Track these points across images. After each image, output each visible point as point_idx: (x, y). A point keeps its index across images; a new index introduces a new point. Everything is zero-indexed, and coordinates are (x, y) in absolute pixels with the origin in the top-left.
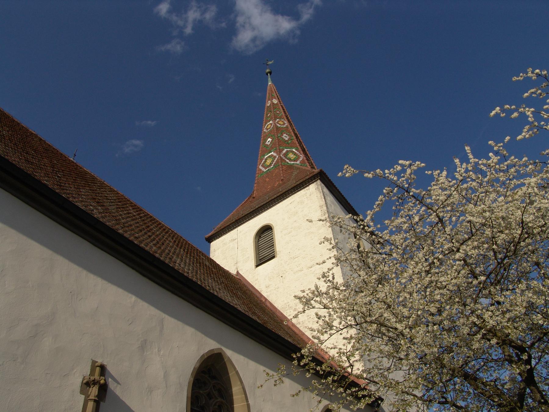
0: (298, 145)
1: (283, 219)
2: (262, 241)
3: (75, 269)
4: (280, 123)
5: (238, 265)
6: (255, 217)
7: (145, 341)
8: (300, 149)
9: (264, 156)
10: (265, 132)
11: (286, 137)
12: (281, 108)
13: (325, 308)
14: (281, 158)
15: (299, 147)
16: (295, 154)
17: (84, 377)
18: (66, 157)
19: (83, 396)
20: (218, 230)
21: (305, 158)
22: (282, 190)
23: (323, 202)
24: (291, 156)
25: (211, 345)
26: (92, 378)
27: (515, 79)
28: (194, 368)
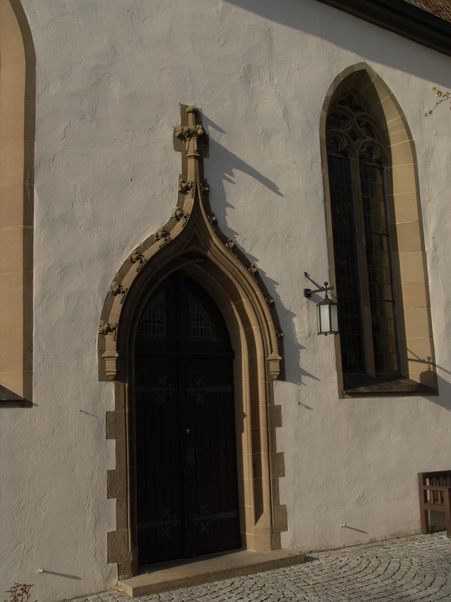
7: (249, 66)
19: (179, 154)
25: (348, 59)
26: (186, 129)
28: (326, 97)
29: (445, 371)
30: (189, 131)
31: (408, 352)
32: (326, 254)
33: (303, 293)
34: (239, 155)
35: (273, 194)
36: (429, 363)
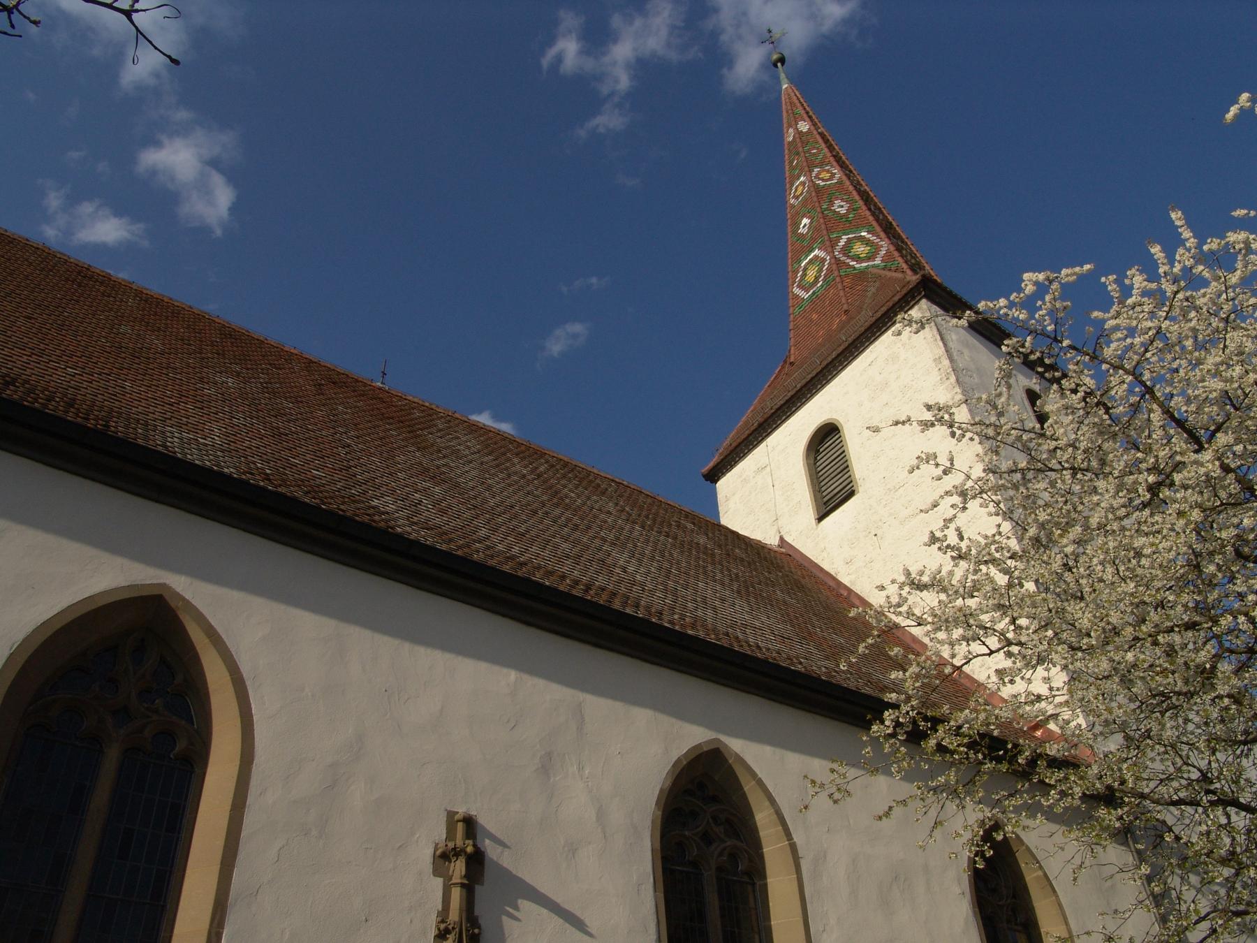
0: (871, 218)
1: (861, 405)
2: (824, 460)
3: (386, 644)
4: (825, 175)
6: (798, 409)
7: (549, 755)
9: (800, 261)
10: (793, 206)
11: (840, 207)
12: (820, 140)
13: (919, 625)
15: (875, 224)
17: (437, 845)
18: (365, 385)
19: (440, 881)
21: (892, 248)
22: (845, 338)
24: (860, 249)
25: (694, 736)
26: (451, 845)
28: (661, 791)
30: (455, 848)
34: (528, 879)
35: (578, 935)
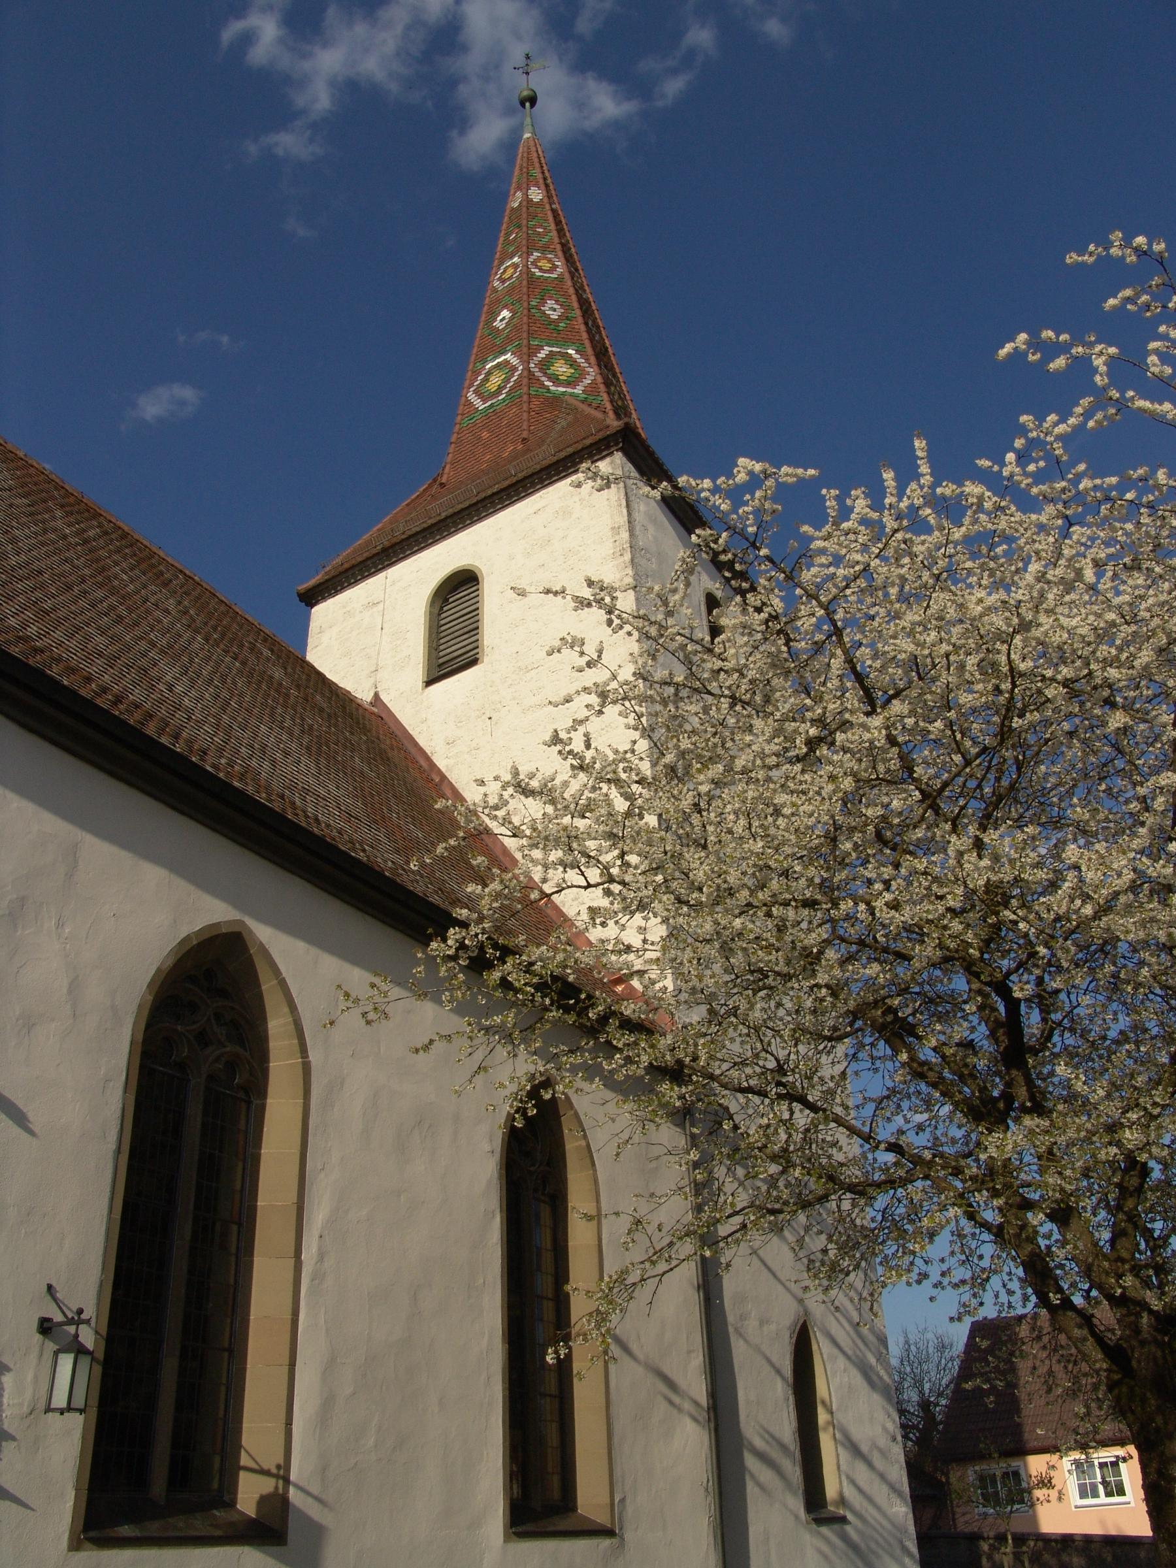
0: (585, 335)
5: (379, 675)
7: (23, 900)
8: (590, 351)
9: (485, 362)
10: (495, 290)
11: (552, 310)
13: (514, 836)
14: (531, 374)
15: (587, 343)
16: (572, 363)
20: (333, 574)
21: (600, 379)
23: (622, 519)
25: (212, 912)
27: (1072, 258)
28: (159, 970)
29: (308, 1493)
31: (243, 1453)
32: (101, 1252)
33: (35, 1325)
35: (15, 1130)
36: (277, 1476)
